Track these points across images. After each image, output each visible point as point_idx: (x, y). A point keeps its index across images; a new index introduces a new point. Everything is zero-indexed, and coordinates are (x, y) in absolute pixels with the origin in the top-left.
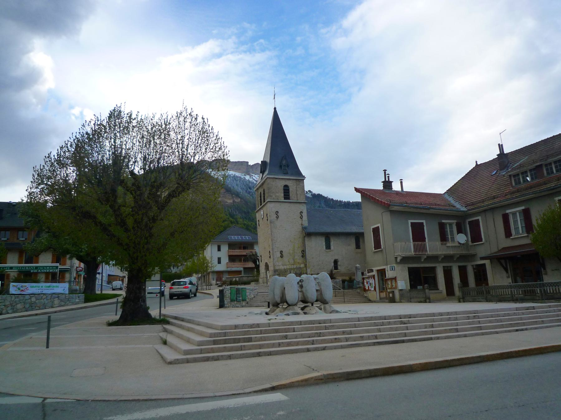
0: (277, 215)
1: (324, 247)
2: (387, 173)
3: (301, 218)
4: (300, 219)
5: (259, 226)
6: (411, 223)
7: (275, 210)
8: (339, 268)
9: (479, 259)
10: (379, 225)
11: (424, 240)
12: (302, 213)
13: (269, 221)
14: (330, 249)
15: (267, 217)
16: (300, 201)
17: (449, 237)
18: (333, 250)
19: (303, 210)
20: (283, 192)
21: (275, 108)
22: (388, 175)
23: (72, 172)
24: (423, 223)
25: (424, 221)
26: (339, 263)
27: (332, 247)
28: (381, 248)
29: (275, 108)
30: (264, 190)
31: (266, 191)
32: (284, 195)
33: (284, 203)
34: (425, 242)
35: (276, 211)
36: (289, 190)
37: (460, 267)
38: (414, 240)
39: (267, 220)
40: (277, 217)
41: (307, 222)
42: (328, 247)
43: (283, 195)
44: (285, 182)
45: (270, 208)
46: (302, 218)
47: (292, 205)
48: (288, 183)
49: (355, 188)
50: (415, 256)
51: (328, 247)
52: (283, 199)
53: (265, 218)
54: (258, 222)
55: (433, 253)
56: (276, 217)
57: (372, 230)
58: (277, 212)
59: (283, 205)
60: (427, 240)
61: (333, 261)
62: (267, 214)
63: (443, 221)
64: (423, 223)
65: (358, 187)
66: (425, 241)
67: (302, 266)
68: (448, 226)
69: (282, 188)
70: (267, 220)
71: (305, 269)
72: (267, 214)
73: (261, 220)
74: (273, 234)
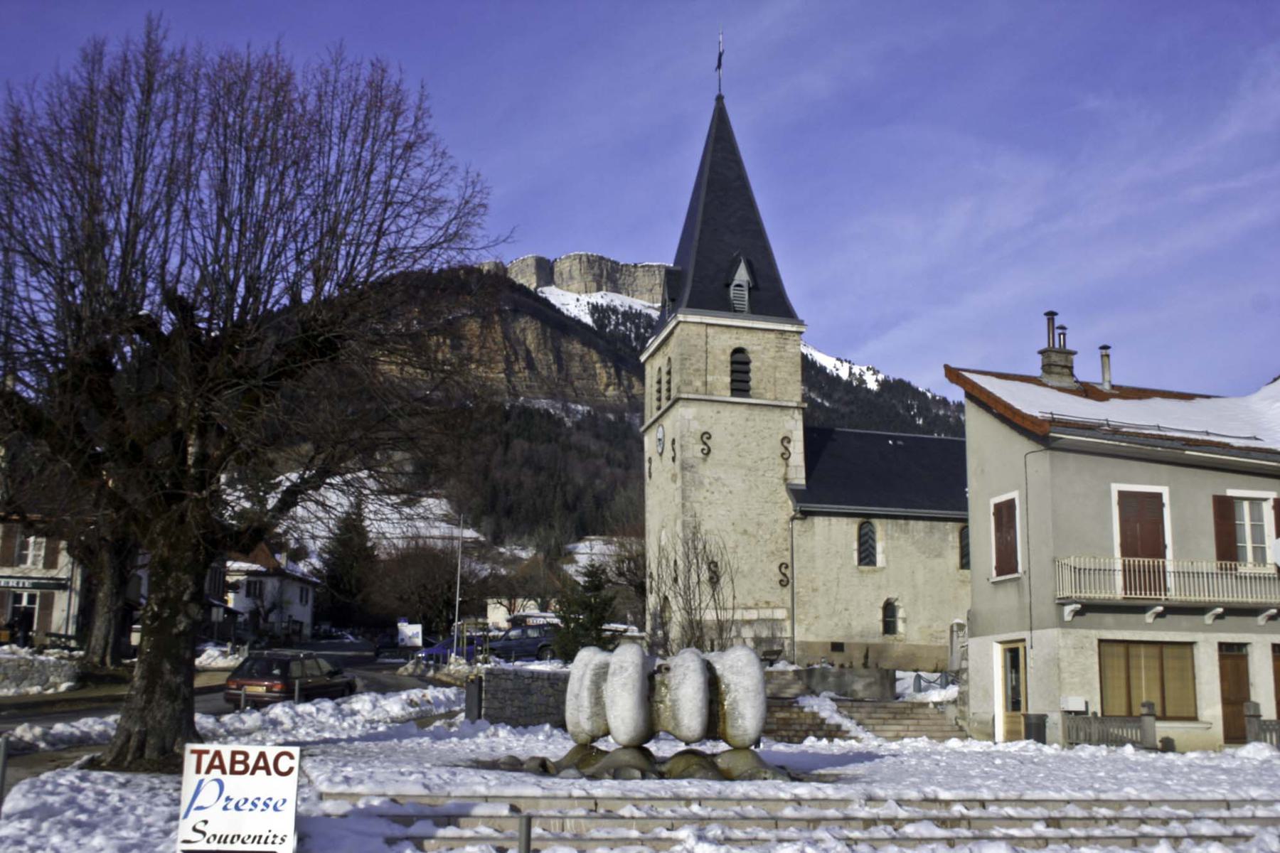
0: (705, 444)
1: (855, 555)
2: (1058, 321)
3: (786, 456)
4: (781, 461)
5: (650, 476)
6: (1123, 495)
7: (697, 428)
8: (901, 627)
9: (889, 637)
10: (1014, 495)
11: (1159, 551)
12: (789, 442)
13: (678, 462)
14: (872, 562)
15: (674, 450)
16: (784, 404)
17: (1249, 545)
18: (884, 568)
19: (791, 432)
20: (729, 369)
21: (720, 99)
22: (1060, 331)
23: (320, 322)
24: (1159, 496)
25: (1165, 491)
26: (901, 613)
27: (880, 559)
28: (1015, 570)
29: (720, 99)
30: (669, 359)
31: (676, 366)
32: (733, 381)
33: (729, 407)
34: (1161, 561)
35: (704, 430)
36: (748, 363)
37: (1224, 648)
38: (1126, 552)
39: (674, 459)
40: (707, 452)
41: (802, 474)
42: (867, 555)
43: (728, 380)
44: (737, 339)
45: (684, 419)
46: (787, 459)
47: (757, 411)
48: (744, 341)
49: (947, 367)
50: (1125, 602)
51: (867, 555)
52: (729, 393)
53: (668, 454)
54: (647, 465)
55: (1188, 598)
56: (703, 450)
57: (992, 510)
58: (706, 436)
59: (727, 412)
60: (1169, 553)
61: (881, 604)
62: (673, 442)
63: (1231, 492)
64: (1159, 496)
65: (953, 365)
66: (1163, 556)
67: (780, 614)
68: (1246, 505)
69: (727, 358)
70: (674, 459)
71: (788, 624)
72: (673, 442)
73: (656, 458)
74: (688, 504)
